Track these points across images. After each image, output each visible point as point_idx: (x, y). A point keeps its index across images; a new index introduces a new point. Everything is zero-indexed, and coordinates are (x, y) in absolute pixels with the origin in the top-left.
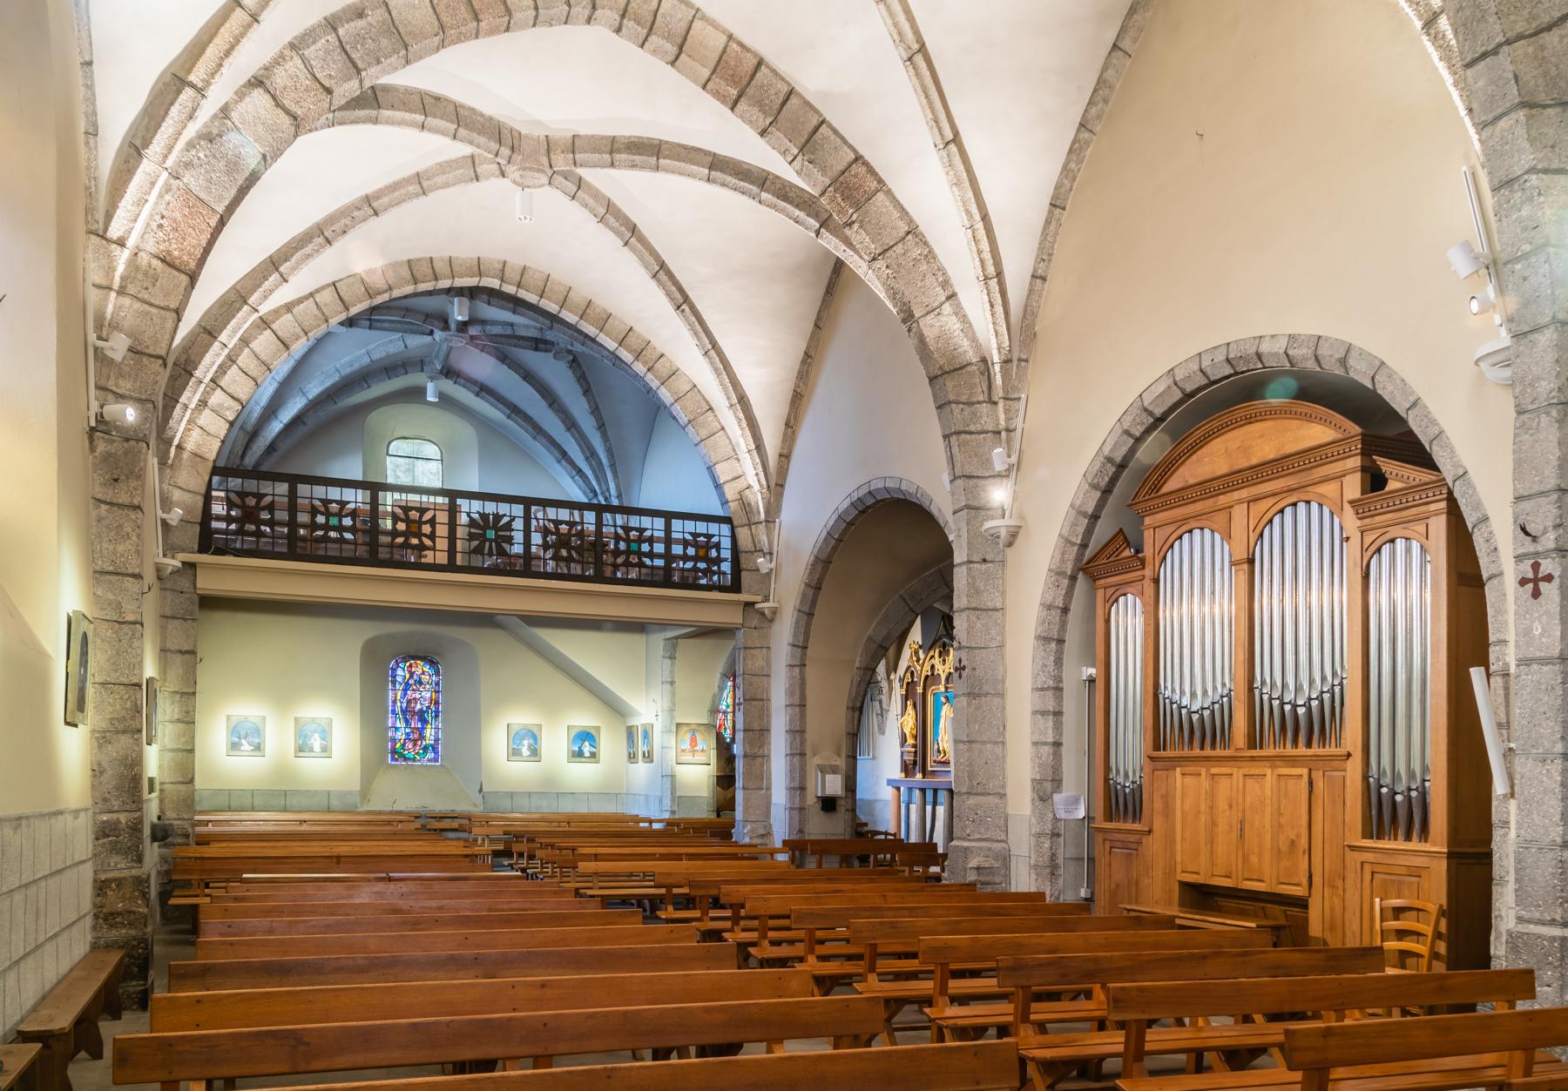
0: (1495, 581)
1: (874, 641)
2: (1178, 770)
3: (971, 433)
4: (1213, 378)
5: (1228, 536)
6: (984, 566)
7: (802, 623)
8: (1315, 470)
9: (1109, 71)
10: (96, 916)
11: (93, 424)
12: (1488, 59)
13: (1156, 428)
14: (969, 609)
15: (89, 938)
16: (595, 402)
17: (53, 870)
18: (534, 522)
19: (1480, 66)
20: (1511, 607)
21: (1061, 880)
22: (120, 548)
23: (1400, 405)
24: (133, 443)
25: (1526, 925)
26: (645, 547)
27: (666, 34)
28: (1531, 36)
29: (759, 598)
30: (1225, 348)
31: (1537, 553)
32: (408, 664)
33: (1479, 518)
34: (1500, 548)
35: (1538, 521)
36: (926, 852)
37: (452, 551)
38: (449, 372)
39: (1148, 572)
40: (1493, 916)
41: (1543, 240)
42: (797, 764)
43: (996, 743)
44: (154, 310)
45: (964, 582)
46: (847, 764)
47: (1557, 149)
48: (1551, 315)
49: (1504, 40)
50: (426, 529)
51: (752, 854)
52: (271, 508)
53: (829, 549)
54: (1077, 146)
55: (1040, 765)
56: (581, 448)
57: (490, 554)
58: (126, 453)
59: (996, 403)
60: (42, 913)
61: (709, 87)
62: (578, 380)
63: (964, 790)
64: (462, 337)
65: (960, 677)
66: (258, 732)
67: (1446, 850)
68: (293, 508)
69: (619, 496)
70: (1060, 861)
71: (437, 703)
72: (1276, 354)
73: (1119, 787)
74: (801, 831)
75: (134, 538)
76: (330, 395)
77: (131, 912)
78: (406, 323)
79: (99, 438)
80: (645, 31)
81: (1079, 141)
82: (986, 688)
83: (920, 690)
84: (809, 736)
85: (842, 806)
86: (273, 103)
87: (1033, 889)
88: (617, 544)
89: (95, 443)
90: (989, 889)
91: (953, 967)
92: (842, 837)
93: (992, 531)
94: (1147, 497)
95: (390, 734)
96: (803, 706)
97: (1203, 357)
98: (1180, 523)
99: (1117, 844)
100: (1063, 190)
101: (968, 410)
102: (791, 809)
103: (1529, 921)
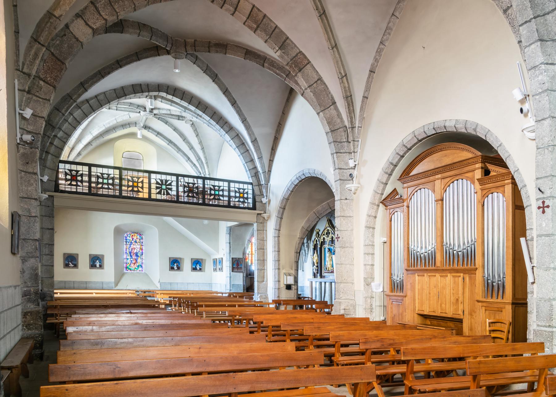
0: (529, 208)
1: (305, 228)
2: (416, 274)
3: (341, 153)
5: (434, 191)
6: (346, 201)
7: (279, 221)
9: (391, 23)
10: (23, 326)
11: (18, 142)
12: (527, 24)
13: (408, 152)
15: (21, 333)
16: (200, 140)
17: (9, 307)
18: (180, 183)
19: (525, 26)
21: (374, 314)
22: (29, 189)
24: (33, 149)
26: (221, 193)
27: (230, 4)
28: (542, 16)
29: (262, 212)
30: (433, 124)
32: (131, 235)
33: (523, 186)
36: (323, 304)
37: (150, 193)
38: (146, 127)
39: (405, 204)
41: (546, 88)
42: (277, 273)
44: (41, 100)
45: (339, 207)
46: (295, 272)
47: (551, 56)
48: (549, 114)
49: (533, 17)
50: (140, 185)
51: (261, 305)
52: (82, 175)
53: (288, 194)
54: (379, 50)
56: (195, 156)
57: (164, 194)
58: (31, 153)
59: (350, 142)
60: (5, 323)
61: (246, 23)
62: (194, 131)
63: (339, 282)
64: (151, 114)
65: (338, 241)
66: (266, 213)
67: (511, 302)
68: (90, 176)
69: (209, 174)
70: (374, 307)
71: (142, 249)
72: (451, 127)
73: (395, 280)
74: (279, 297)
75: (35, 185)
76: (101, 135)
77: (36, 324)
78: (130, 108)
79: (21, 147)
80: (223, 2)
81: (380, 49)
82: (347, 245)
83: (319, 246)
84: (281, 262)
85: (293, 287)
86: (84, 23)
88: (210, 191)
89: (19, 149)
90: (349, 317)
91: (342, 342)
92: (293, 299)
94: (405, 177)
95: (125, 261)
96: (279, 251)
98: (417, 186)
99: (394, 300)
100: (374, 66)
101: (340, 145)
102: (275, 289)
103: (541, 326)
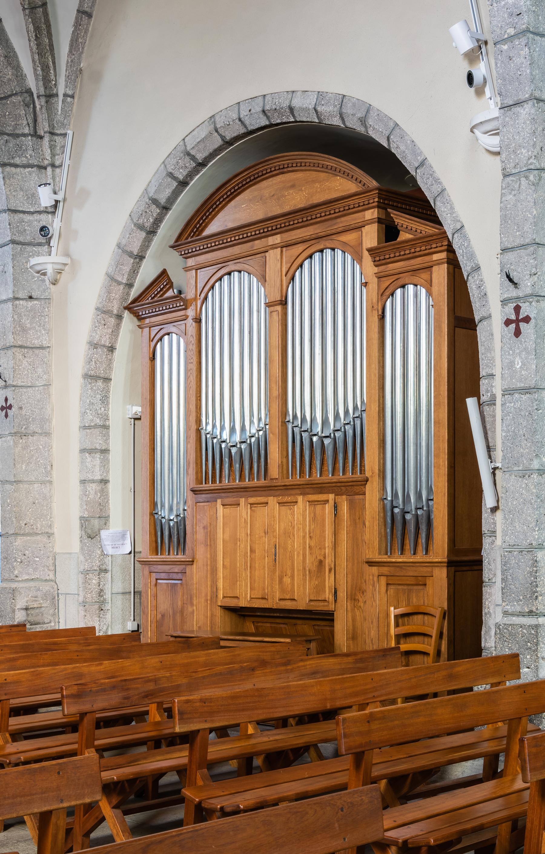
0: (485, 323)
2: (219, 501)
3: (16, 166)
4: (251, 128)
5: (263, 279)
6: (30, 304)
8: (339, 220)
13: (198, 172)
14: (15, 346)
20: (497, 344)
21: (109, 616)
23: (410, 163)
25: (510, 618)
30: (261, 99)
31: (518, 298)
34: (489, 294)
35: (519, 270)
39: (191, 313)
40: (483, 613)
41: (524, 26)
43: (43, 483)
55: (87, 503)
59: (41, 137)
67: (446, 560)
70: (108, 596)
72: (307, 109)
82: (33, 427)
87: (82, 625)
90: (38, 628)
93: (38, 268)
94: (189, 240)
97: (242, 107)
99: (163, 576)
103: (513, 615)
